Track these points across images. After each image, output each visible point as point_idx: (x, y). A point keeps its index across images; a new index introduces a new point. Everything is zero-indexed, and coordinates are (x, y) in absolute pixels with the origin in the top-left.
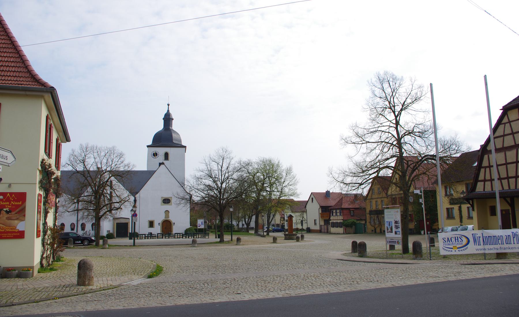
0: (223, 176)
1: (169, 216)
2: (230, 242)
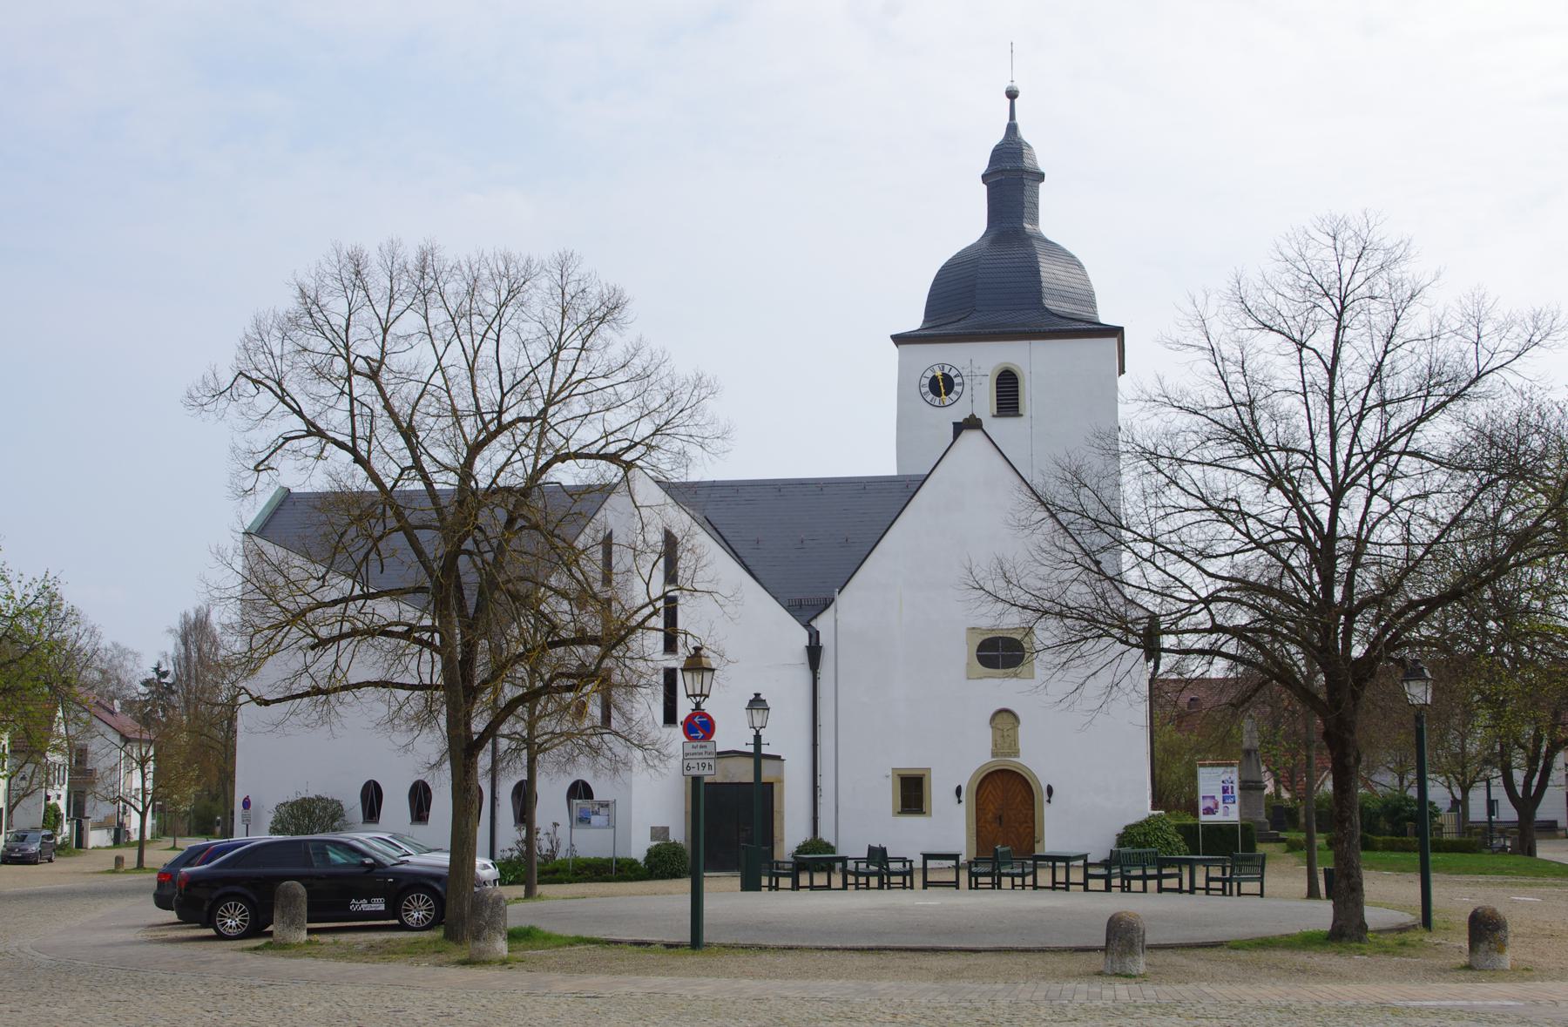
0: (1344, 440)
1: (1015, 742)
2: (1410, 937)
